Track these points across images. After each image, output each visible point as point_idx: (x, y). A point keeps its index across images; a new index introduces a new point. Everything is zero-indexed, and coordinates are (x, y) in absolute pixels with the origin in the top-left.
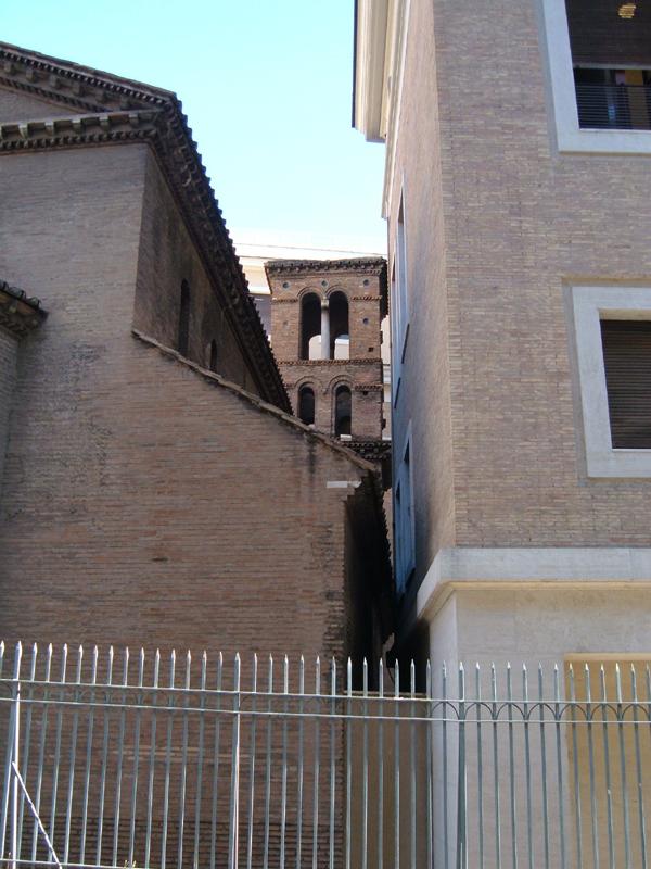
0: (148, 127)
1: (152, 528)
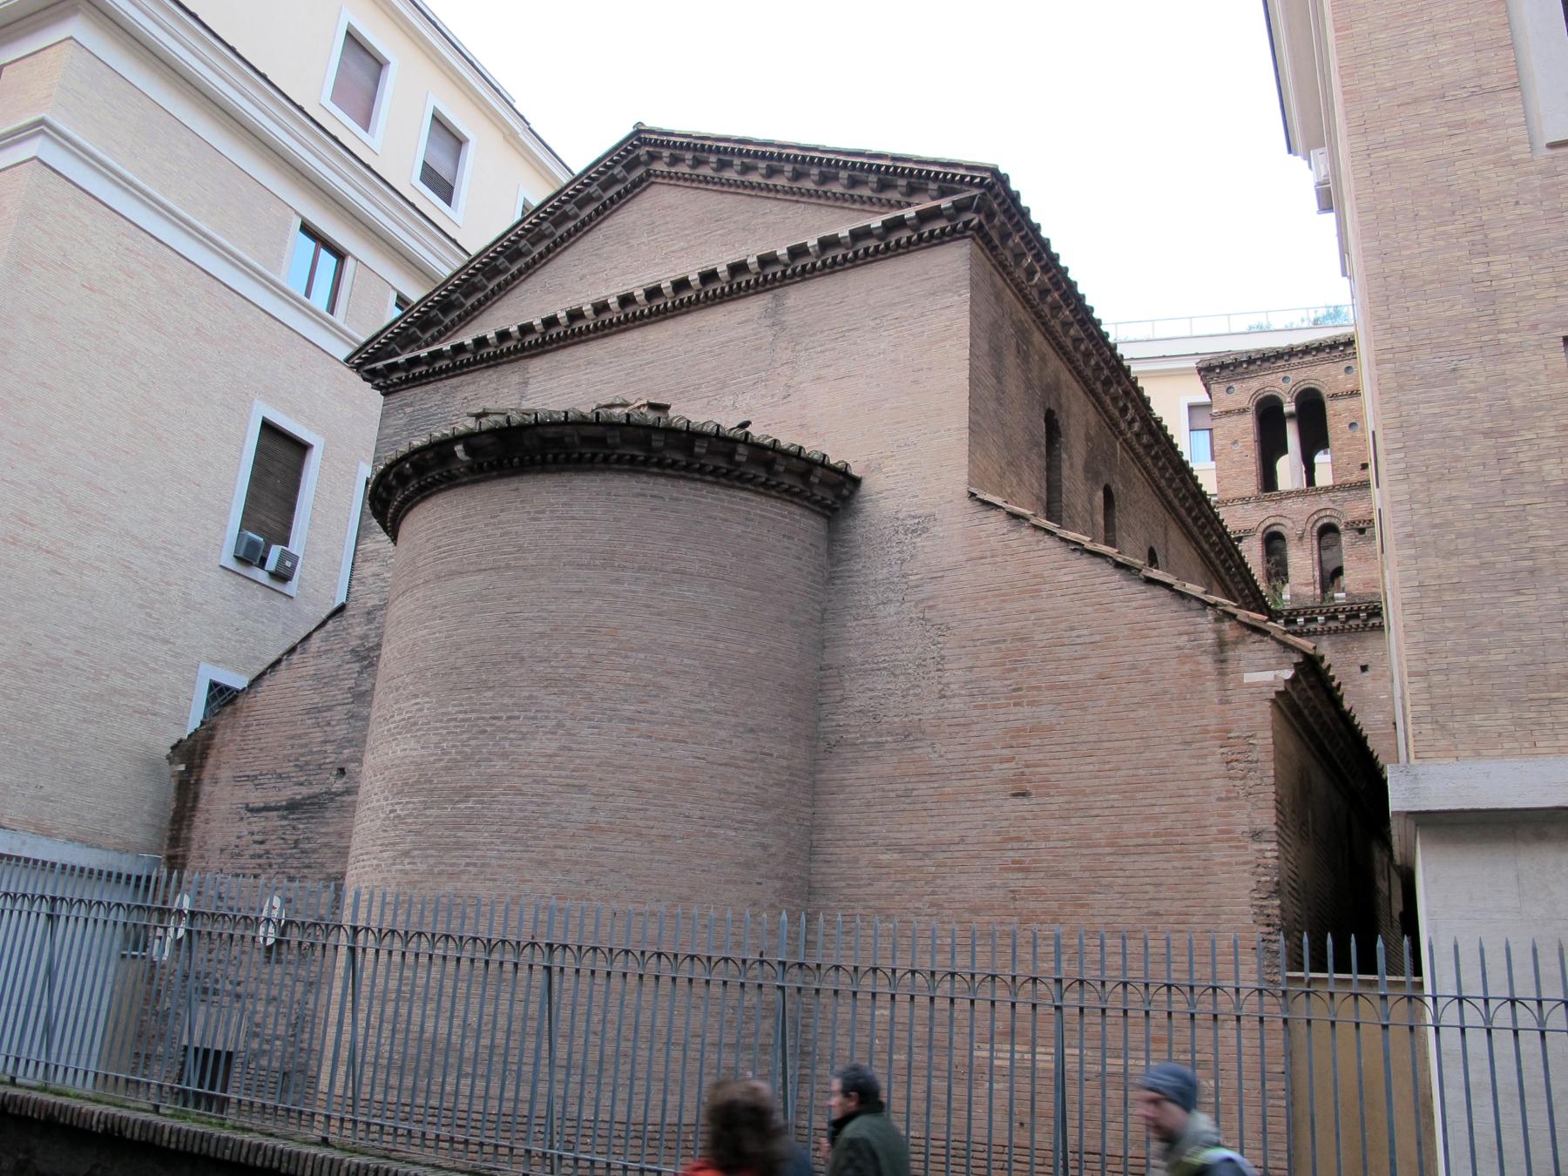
0: (967, 216)
1: (1007, 752)
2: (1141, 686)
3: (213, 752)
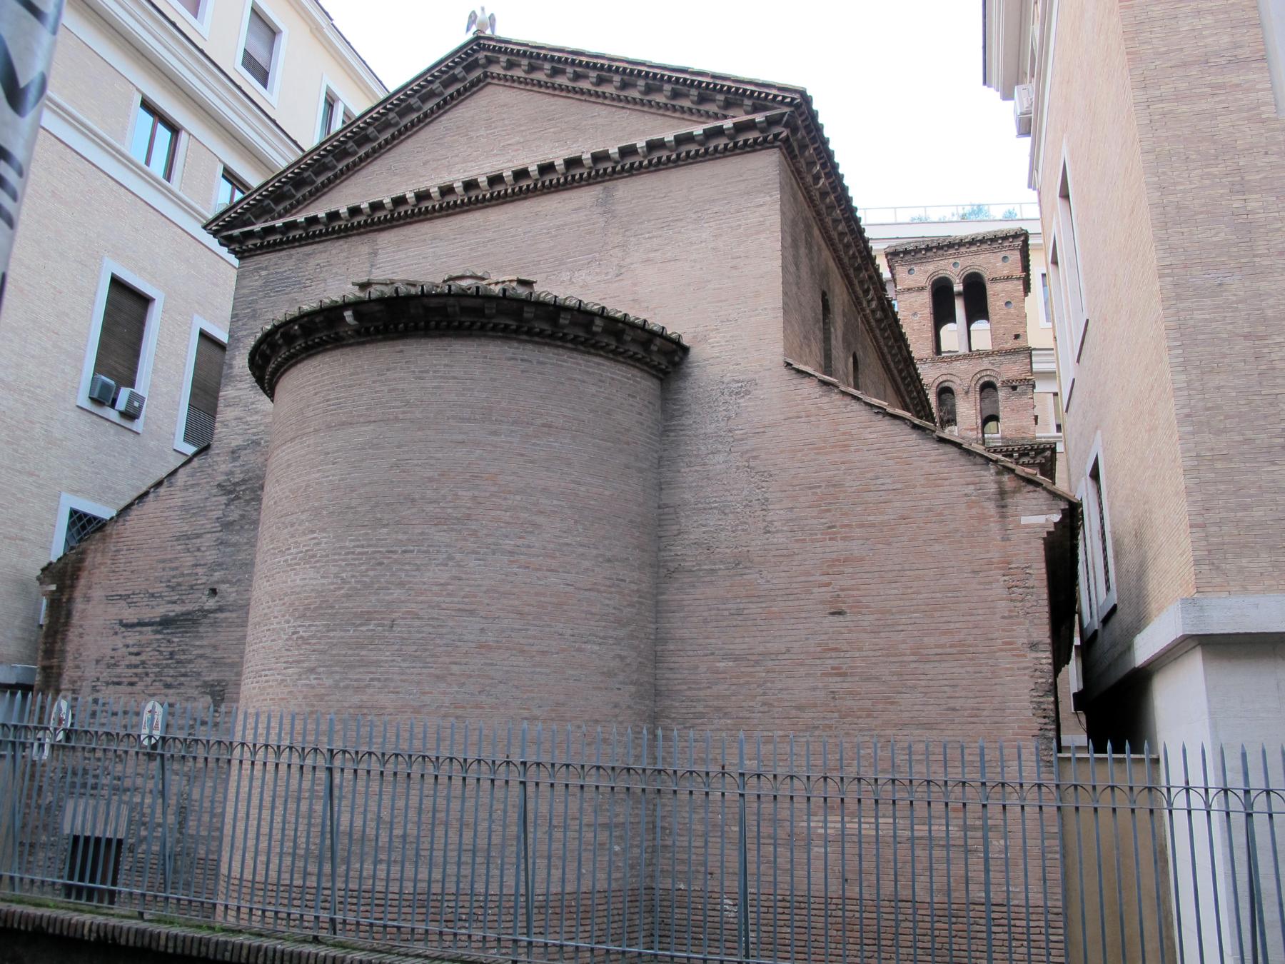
1: (825, 579)
2: (937, 525)
3: (84, 574)
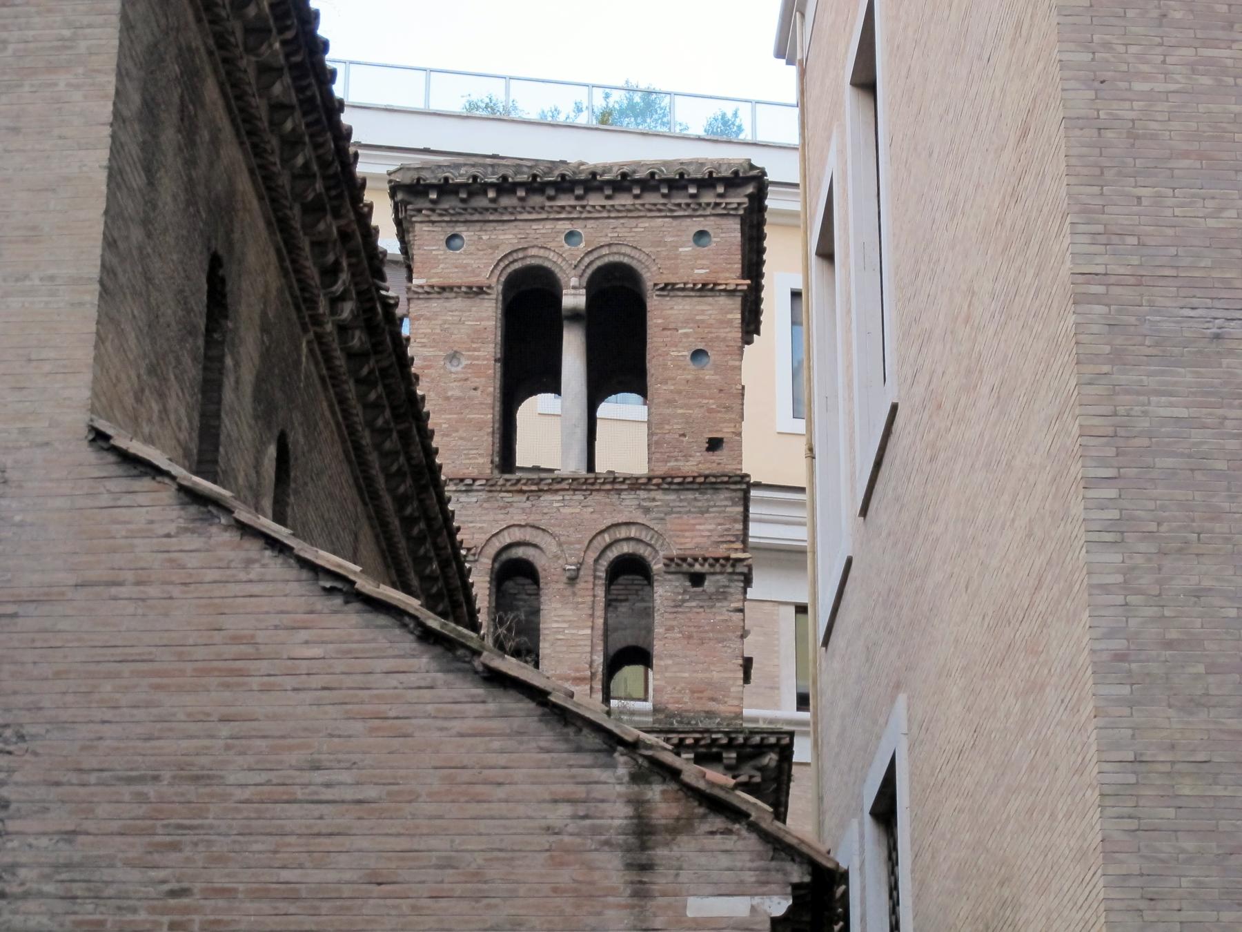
2: (463, 906)
